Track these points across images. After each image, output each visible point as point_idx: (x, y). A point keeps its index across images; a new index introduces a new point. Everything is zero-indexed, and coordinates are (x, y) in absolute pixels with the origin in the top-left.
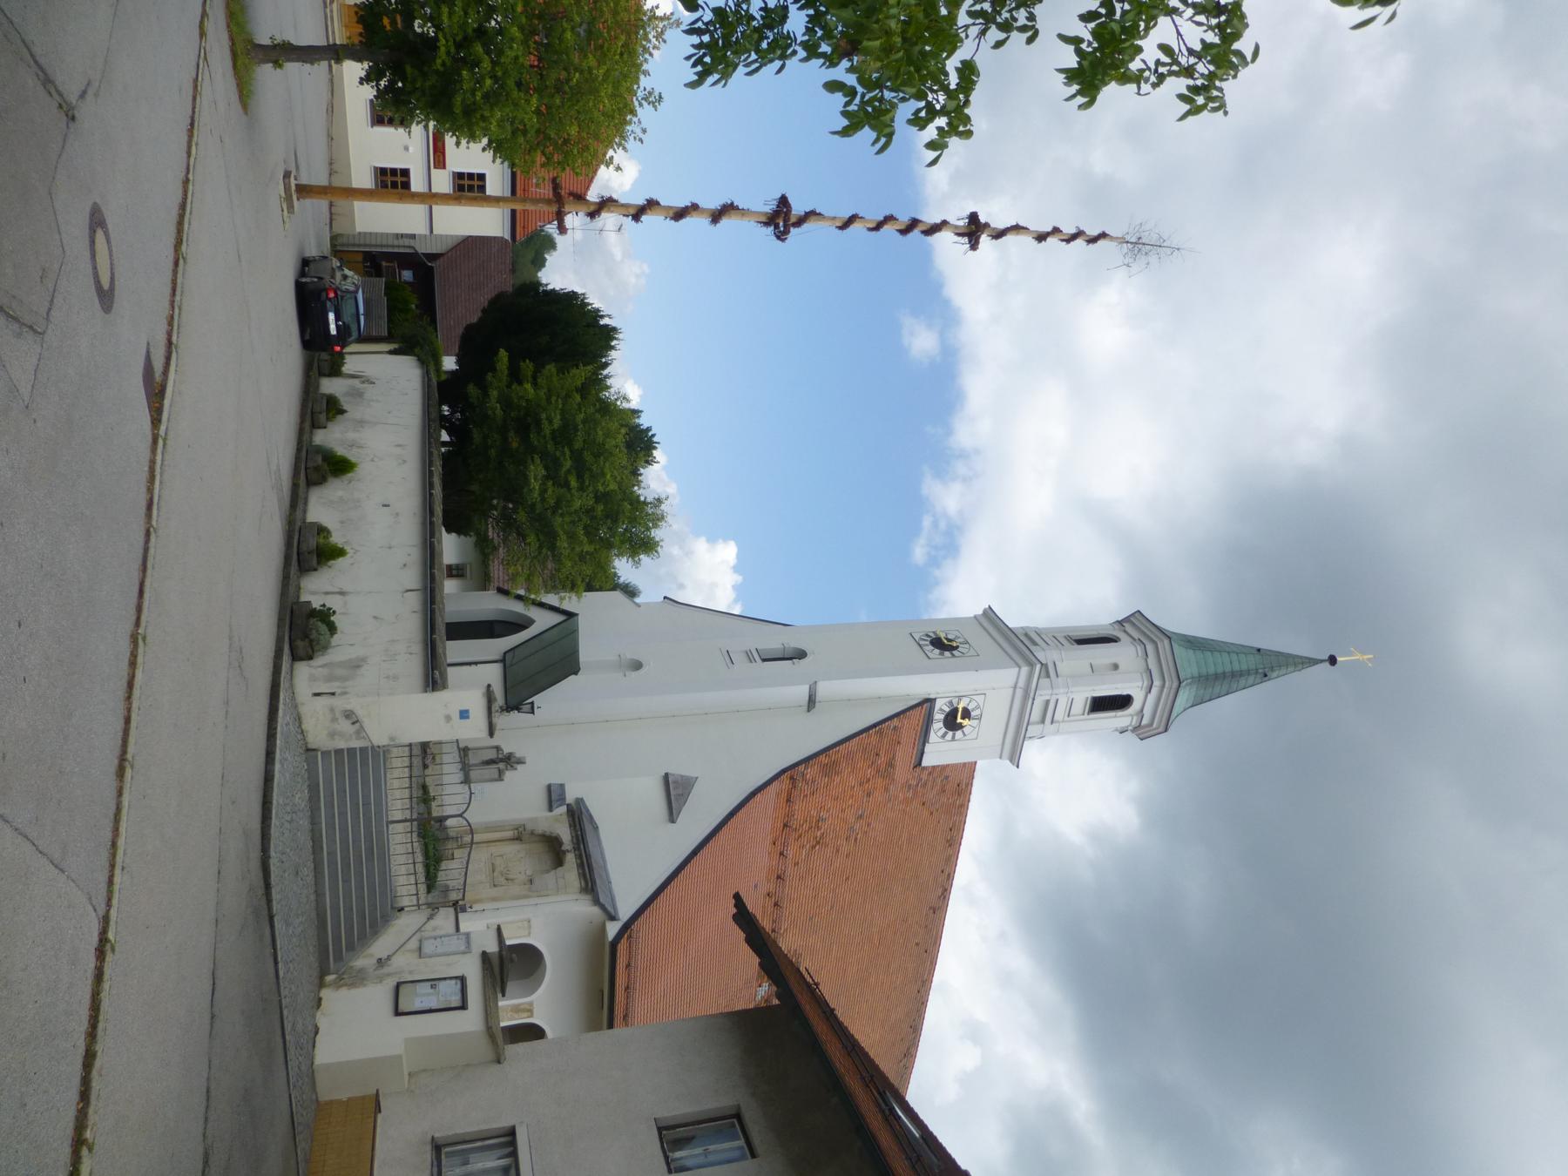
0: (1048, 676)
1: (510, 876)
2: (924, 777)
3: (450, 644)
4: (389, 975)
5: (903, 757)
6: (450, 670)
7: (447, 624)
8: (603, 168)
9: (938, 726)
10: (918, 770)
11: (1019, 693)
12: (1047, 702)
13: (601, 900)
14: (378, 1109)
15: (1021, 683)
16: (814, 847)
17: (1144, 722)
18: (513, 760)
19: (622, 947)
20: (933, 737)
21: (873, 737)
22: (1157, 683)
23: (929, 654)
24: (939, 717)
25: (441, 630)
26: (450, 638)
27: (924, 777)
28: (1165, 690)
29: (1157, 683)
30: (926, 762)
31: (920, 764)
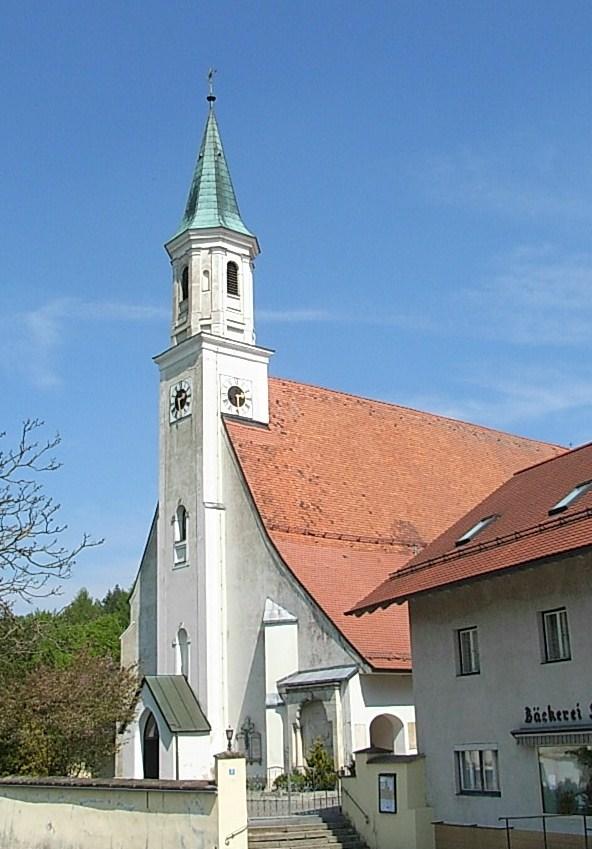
0: (209, 326)
1: (326, 735)
2: (275, 421)
3: (161, 776)
4: (374, 816)
5: (258, 437)
6: (180, 778)
7: (145, 777)
8: (429, 540)
9: (243, 412)
10: (271, 426)
11: (221, 349)
12: (229, 327)
13: (346, 676)
14: (441, 823)
15: (214, 347)
16: (321, 511)
17: (247, 253)
18: (246, 727)
19: (375, 664)
20: (248, 415)
21: (153, 618)
22: (220, 244)
23: (188, 414)
24: (233, 411)
25: (153, 782)
26: (157, 776)
27: (275, 421)
28: (226, 238)
29: (220, 244)
30: (265, 420)
31: (267, 425)
